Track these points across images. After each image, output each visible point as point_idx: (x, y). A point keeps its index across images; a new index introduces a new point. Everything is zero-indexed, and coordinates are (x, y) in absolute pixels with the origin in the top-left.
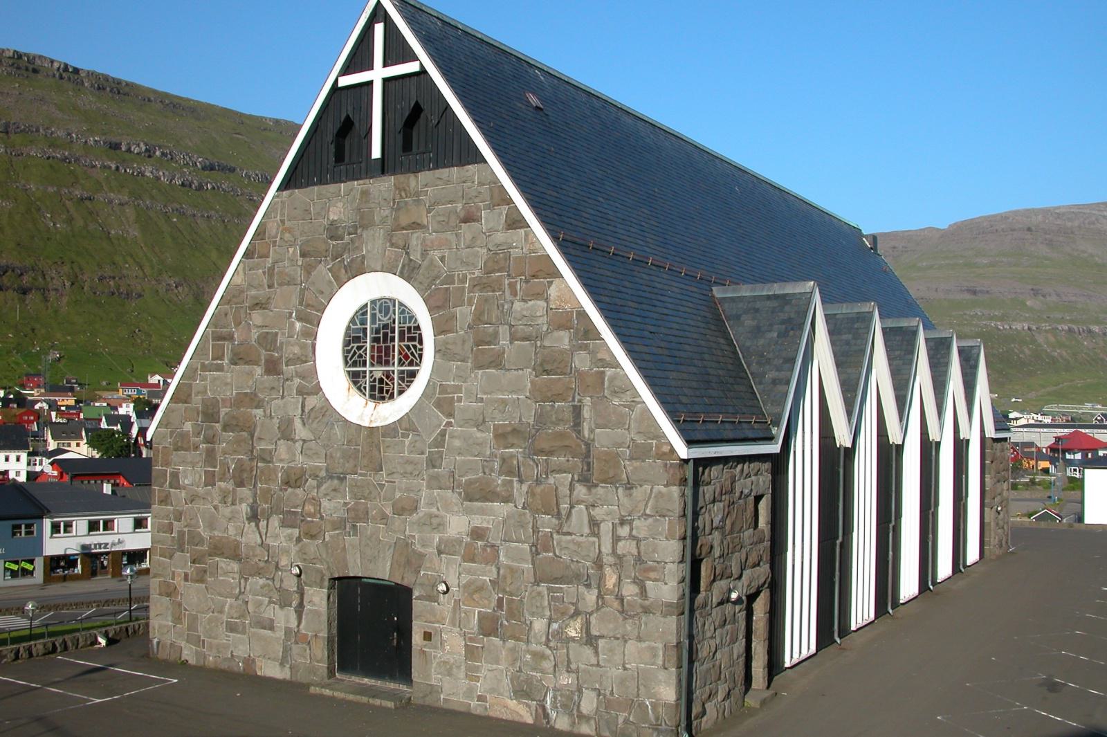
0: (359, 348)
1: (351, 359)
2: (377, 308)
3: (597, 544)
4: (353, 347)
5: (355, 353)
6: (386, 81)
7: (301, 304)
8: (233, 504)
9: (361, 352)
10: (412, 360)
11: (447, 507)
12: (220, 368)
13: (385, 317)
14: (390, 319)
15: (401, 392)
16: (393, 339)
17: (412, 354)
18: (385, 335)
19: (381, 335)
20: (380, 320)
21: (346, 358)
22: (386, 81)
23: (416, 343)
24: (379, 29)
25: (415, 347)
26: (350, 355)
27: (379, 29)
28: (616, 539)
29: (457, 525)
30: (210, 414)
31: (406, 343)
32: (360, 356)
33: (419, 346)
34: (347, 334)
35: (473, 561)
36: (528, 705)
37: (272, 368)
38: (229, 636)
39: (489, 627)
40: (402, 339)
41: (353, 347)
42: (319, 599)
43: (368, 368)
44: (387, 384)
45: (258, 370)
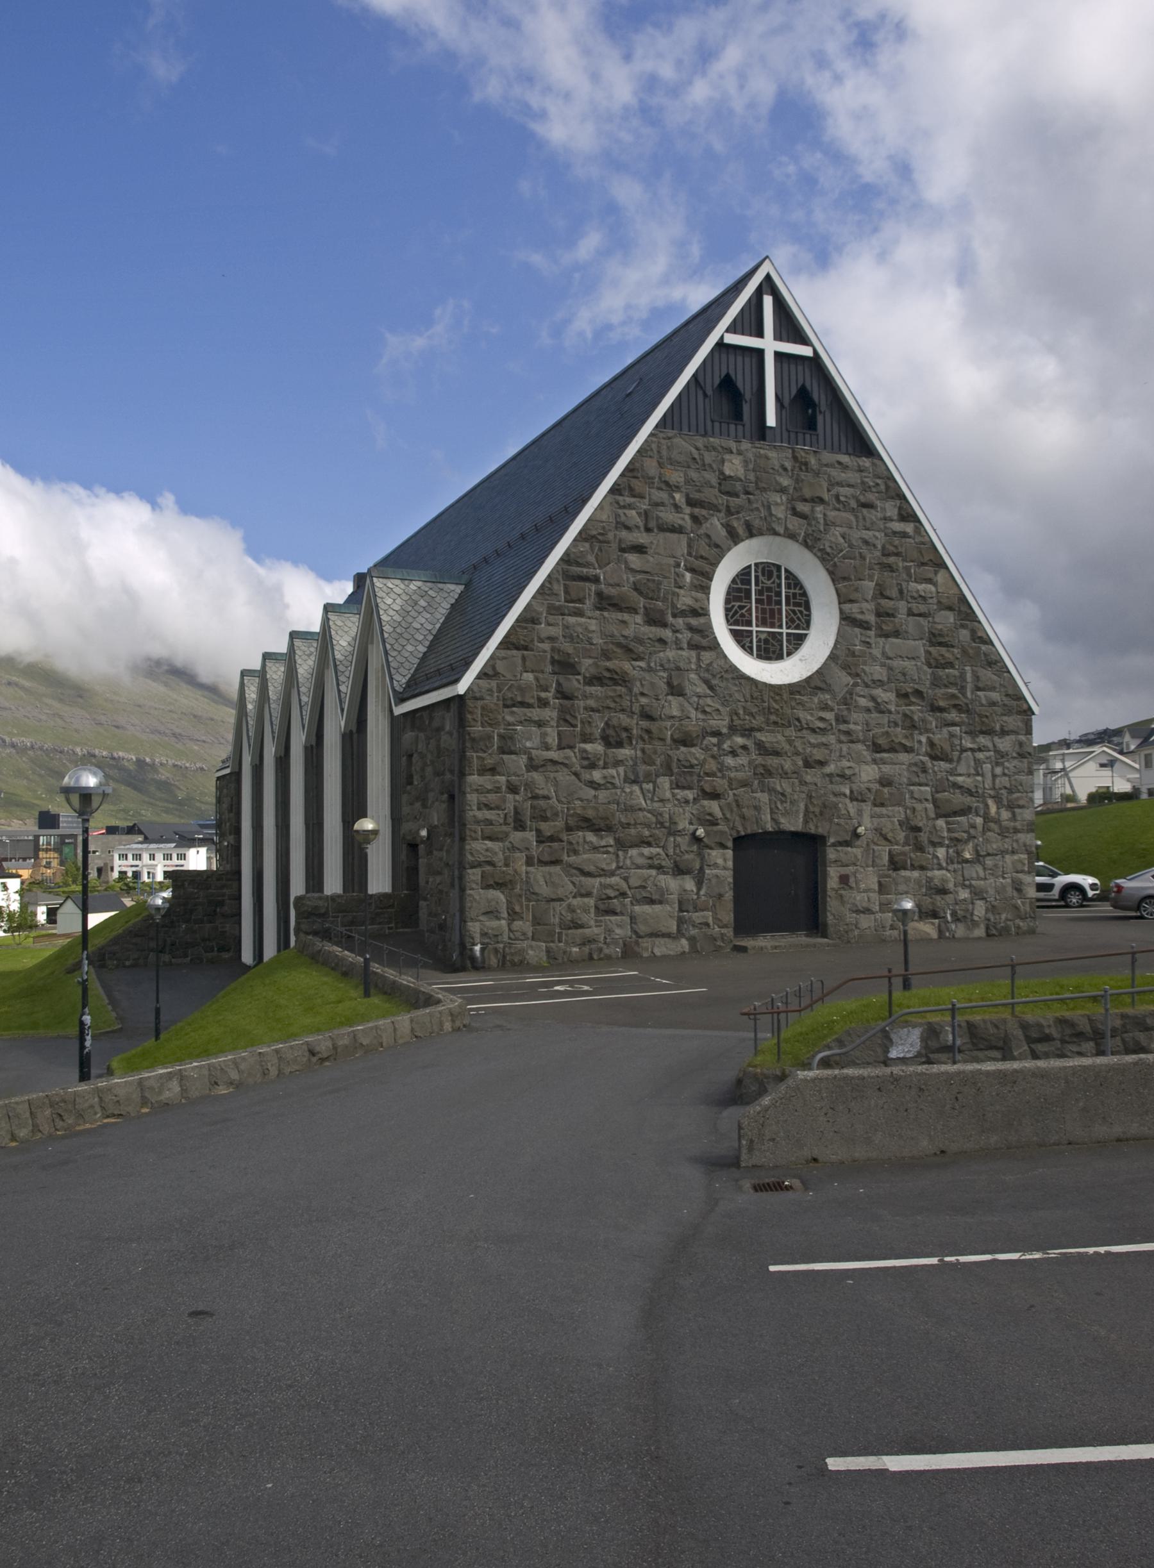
0: (741, 608)
1: (732, 617)
2: (760, 570)
3: (80, 838)
4: (733, 606)
5: (736, 612)
6: (760, 353)
7: (690, 554)
8: (604, 768)
9: (743, 611)
10: (798, 625)
11: (861, 761)
12: (579, 613)
13: (769, 580)
14: (773, 583)
15: (789, 654)
16: (779, 603)
17: (798, 618)
18: (769, 598)
19: (765, 597)
20: (763, 583)
21: (727, 615)
22: (760, 353)
23: (802, 609)
24: (768, 301)
25: (801, 612)
26: (731, 614)
27: (768, 301)
28: (994, 776)
29: (868, 773)
30: (565, 666)
31: (792, 608)
32: (742, 615)
33: (805, 612)
34: (728, 593)
35: (882, 805)
36: (933, 924)
37: (654, 619)
38: (601, 921)
39: (896, 864)
40: (788, 604)
41: (733, 606)
42: (722, 861)
43: (754, 629)
44: (773, 645)
45: (639, 619)
